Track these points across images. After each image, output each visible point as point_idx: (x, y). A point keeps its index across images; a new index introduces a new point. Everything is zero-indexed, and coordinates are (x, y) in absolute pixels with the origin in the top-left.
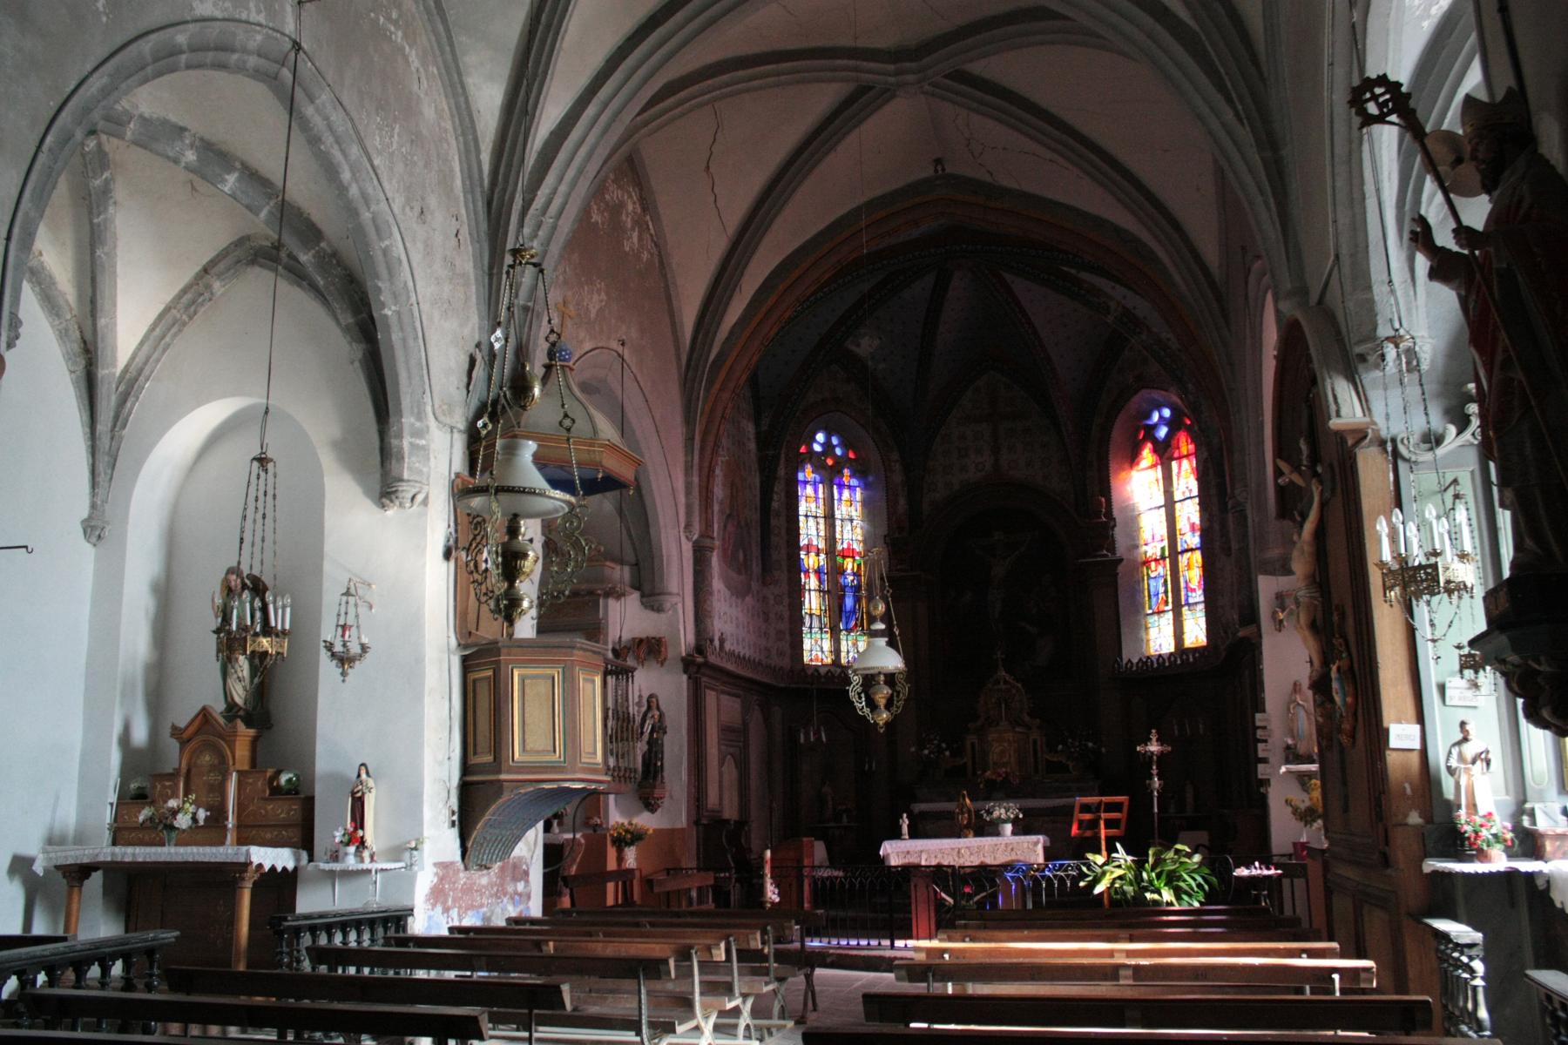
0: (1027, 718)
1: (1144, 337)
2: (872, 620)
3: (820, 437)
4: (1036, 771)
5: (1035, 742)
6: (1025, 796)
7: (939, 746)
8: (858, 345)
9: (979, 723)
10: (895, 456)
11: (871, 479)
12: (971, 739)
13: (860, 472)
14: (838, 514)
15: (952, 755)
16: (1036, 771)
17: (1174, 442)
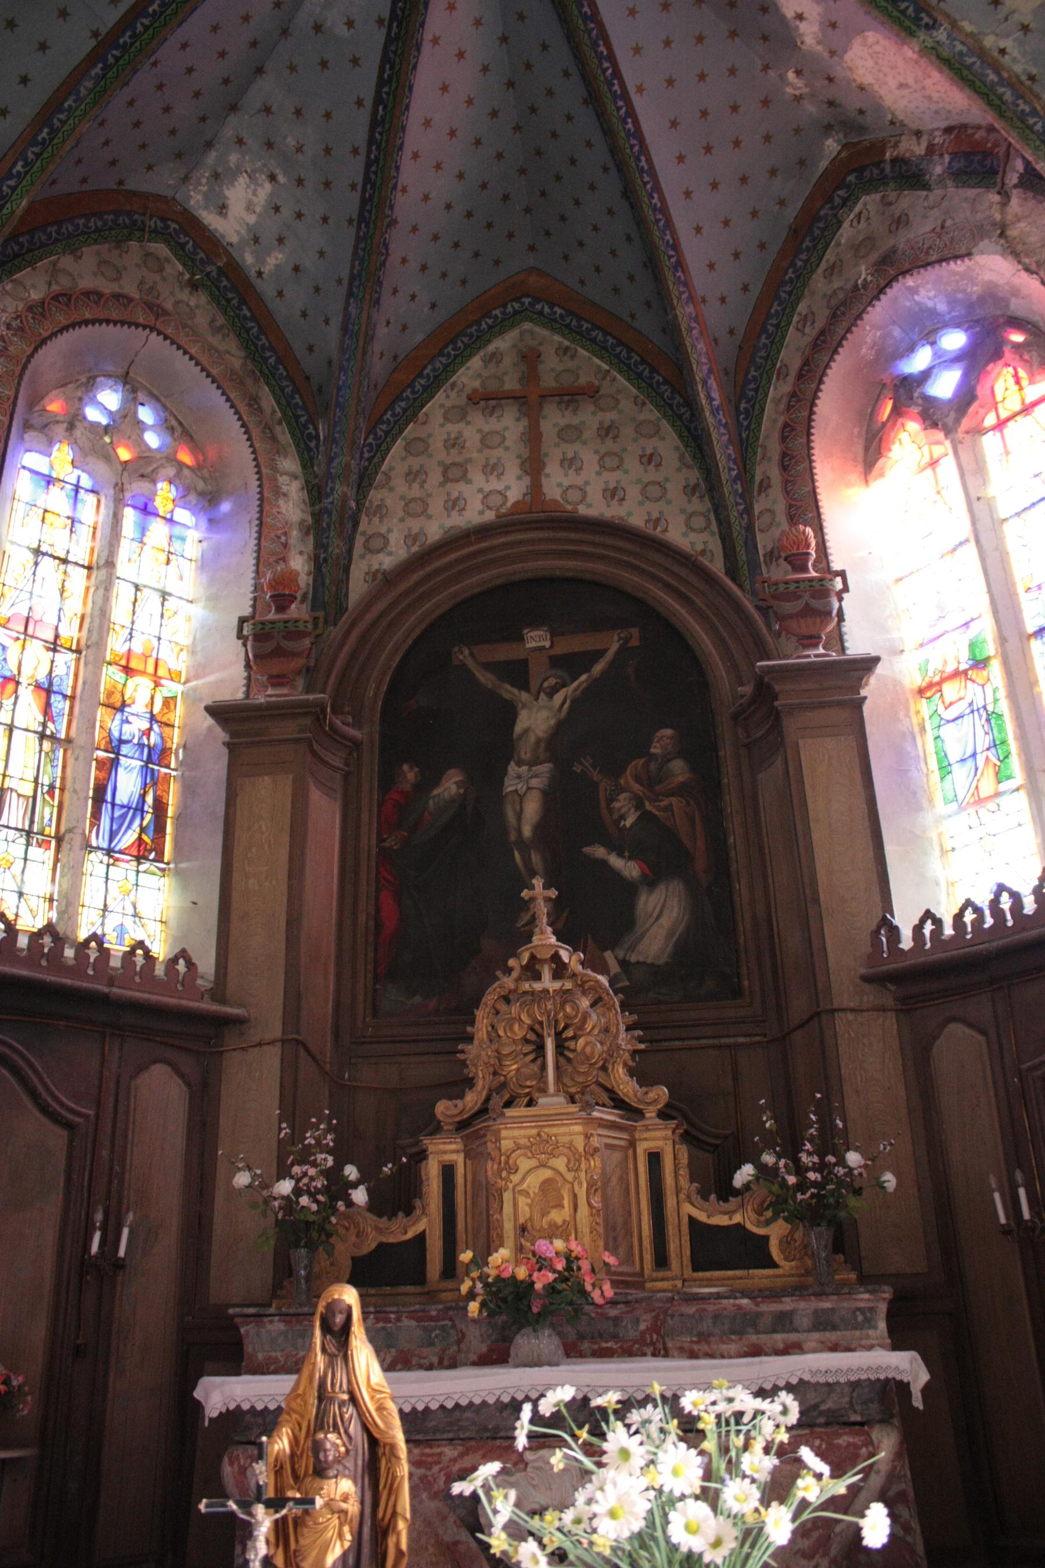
0: (627, 1086)
1: (941, 35)
2: (345, 1216)
3: (110, 398)
4: (661, 1260)
5: (654, 1159)
6: (223, 1513)
7: (333, 1175)
8: (222, 209)
9: (472, 1100)
10: (290, 464)
11: (226, 507)
12: (445, 1150)
13: (206, 493)
14: (123, 568)
15: (375, 1206)
16: (661, 1260)
17: (981, 391)
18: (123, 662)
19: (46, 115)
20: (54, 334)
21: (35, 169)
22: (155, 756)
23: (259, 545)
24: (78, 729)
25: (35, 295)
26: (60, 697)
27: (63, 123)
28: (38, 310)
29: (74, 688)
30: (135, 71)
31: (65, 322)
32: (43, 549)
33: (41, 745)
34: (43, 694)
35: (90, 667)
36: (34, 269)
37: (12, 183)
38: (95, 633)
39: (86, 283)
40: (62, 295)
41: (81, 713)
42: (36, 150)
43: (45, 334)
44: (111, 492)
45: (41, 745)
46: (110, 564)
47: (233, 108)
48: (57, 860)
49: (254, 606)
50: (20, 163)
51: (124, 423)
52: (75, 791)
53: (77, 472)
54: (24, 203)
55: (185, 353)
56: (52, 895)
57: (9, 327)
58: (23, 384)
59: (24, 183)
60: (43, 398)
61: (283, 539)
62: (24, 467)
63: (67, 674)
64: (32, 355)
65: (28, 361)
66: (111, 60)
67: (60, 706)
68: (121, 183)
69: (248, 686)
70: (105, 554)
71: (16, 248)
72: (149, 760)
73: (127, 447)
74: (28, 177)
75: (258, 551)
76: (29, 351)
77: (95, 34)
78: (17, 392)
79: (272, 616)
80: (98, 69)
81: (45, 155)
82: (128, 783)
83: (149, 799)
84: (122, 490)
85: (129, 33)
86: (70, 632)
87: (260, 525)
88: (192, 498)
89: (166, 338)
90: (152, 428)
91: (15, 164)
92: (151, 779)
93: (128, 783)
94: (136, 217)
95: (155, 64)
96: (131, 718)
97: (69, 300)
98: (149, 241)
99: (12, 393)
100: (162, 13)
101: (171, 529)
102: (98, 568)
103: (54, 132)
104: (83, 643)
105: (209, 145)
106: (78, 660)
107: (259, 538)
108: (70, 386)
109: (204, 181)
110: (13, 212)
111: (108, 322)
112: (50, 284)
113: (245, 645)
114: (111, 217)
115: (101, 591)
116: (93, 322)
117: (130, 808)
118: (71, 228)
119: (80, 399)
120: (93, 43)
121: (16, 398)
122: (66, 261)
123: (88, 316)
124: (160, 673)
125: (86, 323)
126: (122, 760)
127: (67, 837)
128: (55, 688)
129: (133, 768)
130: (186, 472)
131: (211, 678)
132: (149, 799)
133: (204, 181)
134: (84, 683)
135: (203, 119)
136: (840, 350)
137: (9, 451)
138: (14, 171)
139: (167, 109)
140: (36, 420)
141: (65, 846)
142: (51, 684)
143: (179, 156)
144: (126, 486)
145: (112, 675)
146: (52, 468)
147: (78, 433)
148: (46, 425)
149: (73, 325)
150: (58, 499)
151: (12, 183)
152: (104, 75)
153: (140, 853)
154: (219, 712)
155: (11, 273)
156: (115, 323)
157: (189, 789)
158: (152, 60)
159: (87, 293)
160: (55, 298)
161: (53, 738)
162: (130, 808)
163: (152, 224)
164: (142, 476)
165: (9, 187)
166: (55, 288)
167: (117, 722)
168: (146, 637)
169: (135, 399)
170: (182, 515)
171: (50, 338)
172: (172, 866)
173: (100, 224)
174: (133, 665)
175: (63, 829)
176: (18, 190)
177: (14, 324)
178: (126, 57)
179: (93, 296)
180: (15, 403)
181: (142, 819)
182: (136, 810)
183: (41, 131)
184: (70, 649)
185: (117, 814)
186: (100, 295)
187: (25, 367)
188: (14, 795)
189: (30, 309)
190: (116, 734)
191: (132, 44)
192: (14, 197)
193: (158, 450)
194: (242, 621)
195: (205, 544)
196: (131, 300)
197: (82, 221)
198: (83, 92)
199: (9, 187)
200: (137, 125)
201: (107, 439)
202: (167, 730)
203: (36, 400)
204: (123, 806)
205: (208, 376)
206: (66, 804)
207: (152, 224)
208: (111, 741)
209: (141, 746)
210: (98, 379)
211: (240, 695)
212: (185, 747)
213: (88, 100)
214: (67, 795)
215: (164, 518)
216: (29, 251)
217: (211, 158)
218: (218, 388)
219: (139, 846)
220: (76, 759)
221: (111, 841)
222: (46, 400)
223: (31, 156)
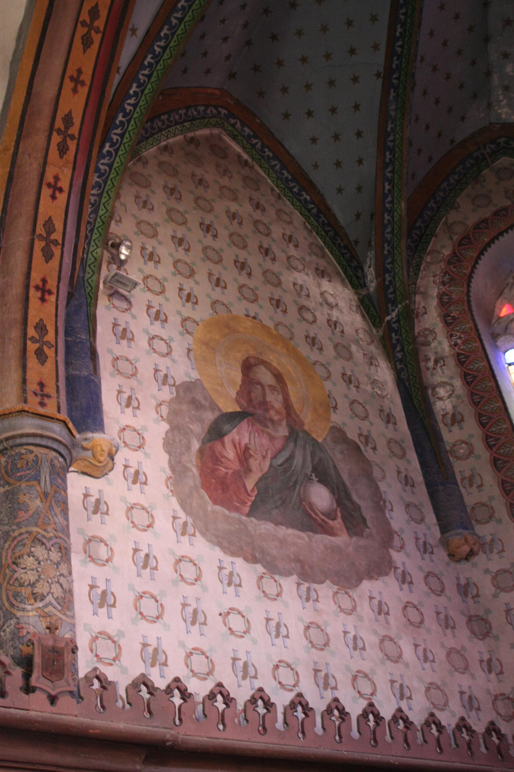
19: (382, 146)
20: (474, 267)
21: (396, 181)
25: (447, 252)
27: (394, 141)
28: (455, 260)
30: (413, 76)
31: (475, 255)
36: (436, 236)
37: (389, 199)
39: (472, 220)
40: (462, 239)
42: (390, 169)
43: (467, 272)
47: (487, 40)
50: (386, 184)
54: (403, 205)
57: (443, 284)
58: (475, 313)
59: (396, 194)
60: (493, 311)
62: (510, 365)
64: (468, 291)
65: (469, 296)
66: (395, 82)
68: (452, 142)
71: (418, 232)
74: (396, 189)
76: (465, 290)
77: (378, 75)
78: (474, 320)
80: (392, 94)
81: (397, 168)
85: (395, 58)
91: (384, 187)
94: (476, 154)
95: (422, 59)
97: (469, 239)
98: (493, 162)
99: (471, 324)
100: (405, 30)
103: (392, 151)
105: (489, 74)
108: (506, 290)
109: (501, 97)
110: (400, 216)
111: (501, 234)
112: (451, 238)
114: (461, 167)
116: (492, 241)
118: (441, 194)
120: (380, 80)
121: (476, 325)
122: (453, 216)
123: (486, 240)
125: (488, 245)
133: (501, 97)
135: (473, 63)
136: (479, 261)
137: (492, 363)
138: (386, 191)
139: (448, 77)
140: (498, 329)
143: (475, 96)
148: (506, 328)
149: (482, 253)
151: (389, 199)
152: (398, 94)
155: (425, 249)
156: (506, 231)
158: (419, 58)
159: (477, 226)
160: (460, 244)
163: (488, 150)
165: (389, 203)
166: (455, 238)
171: (472, 272)
173: (456, 177)
176: (395, 201)
177: (446, 280)
178: (403, 73)
179: (482, 225)
180: (477, 330)
183: (385, 155)
186: (485, 221)
187: (469, 301)
189: (449, 263)
191: (401, 63)
192: (396, 206)
196: (506, 209)
197: (445, 185)
198: (393, 113)
199: (389, 203)
200: (437, 102)
203: (490, 316)
207: (488, 150)
213: (399, 116)
216: (426, 227)
217: (495, 80)
222: (497, 310)
223: (389, 175)
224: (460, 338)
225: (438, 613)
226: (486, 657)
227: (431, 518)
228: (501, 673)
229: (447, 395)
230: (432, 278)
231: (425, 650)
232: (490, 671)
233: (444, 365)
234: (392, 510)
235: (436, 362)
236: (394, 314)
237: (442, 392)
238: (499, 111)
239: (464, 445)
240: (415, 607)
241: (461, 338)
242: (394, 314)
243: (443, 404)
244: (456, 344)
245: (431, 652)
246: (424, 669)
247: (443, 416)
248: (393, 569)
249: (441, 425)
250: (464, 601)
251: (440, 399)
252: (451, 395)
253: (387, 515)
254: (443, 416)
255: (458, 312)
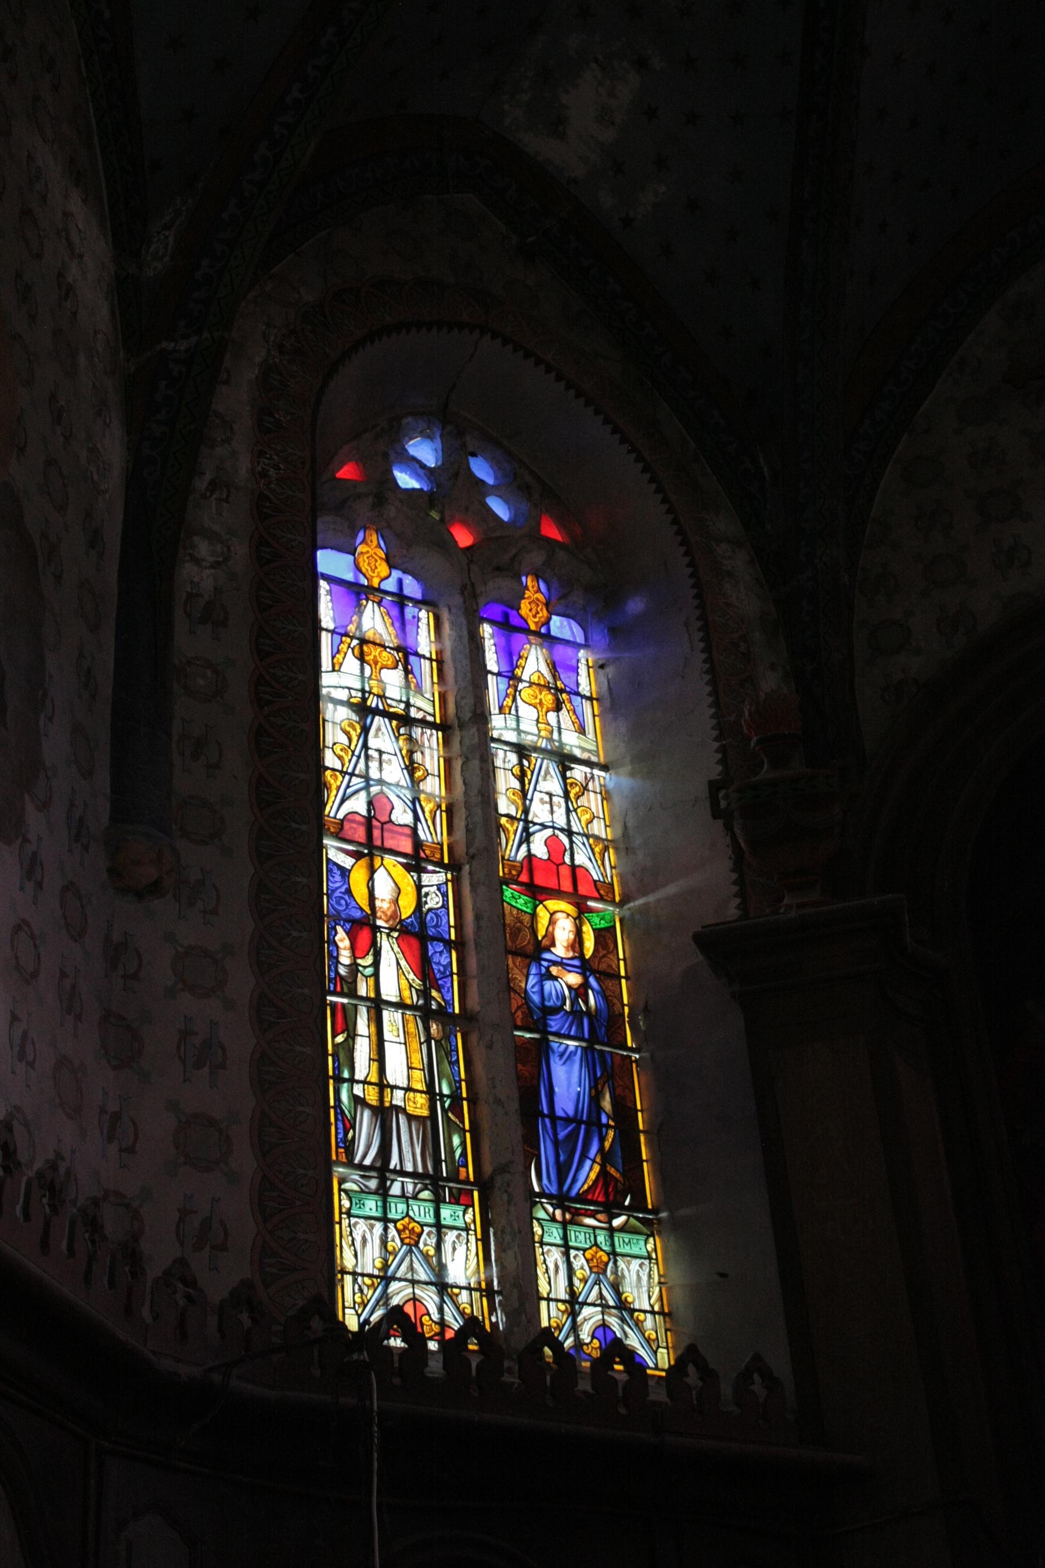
11: (636, 606)
18: (524, 878)
22: (600, 1030)
23: (709, 660)
24: (481, 995)
26: (440, 947)
29: (459, 927)
32: (372, 702)
33: (427, 1029)
34: (415, 943)
35: (482, 889)
38: (479, 834)
41: (482, 968)
44: (458, 600)
45: (427, 1029)
46: (481, 717)
48: (486, 1224)
49: (723, 762)
51: (450, 485)
52: (498, 1102)
53: (396, 574)
55: (539, 362)
56: (489, 1283)
61: (743, 646)
63: (445, 906)
67: (444, 961)
69: (742, 894)
70: (469, 701)
72: (593, 1040)
73: (465, 523)
75: (711, 671)
79: (766, 772)
82: (568, 1082)
83: (607, 1104)
84: (475, 596)
86: (433, 833)
87: (705, 628)
88: (578, 598)
89: (506, 342)
90: (495, 490)
92: (605, 1073)
93: (568, 1082)
96: (554, 970)
101: (550, 650)
102: (461, 726)
104: (461, 850)
106: (456, 882)
107: (707, 649)
113: (729, 828)
115: (475, 764)
117: (580, 1122)
119: (386, 455)
124: (582, 890)
126: (555, 1042)
127: (499, 1181)
128: (431, 932)
129: (573, 1054)
130: (561, 555)
131: (671, 890)
132: (607, 1104)
134: (478, 917)
141: (499, 1198)
142: (423, 923)
144: (480, 588)
145: (515, 899)
146: (358, 568)
147: (391, 511)
150: (373, 620)
153: (609, 1197)
154: (712, 942)
157: (667, 1081)
161: (442, 1014)
162: (580, 1122)
164: (498, 569)
167: (532, 980)
168: (549, 832)
169: (464, 446)
170: (559, 626)
172: (663, 1215)
174: (539, 880)
175: (488, 1169)
181: (602, 1140)
182: (589, 1124)
184: (440, 864)
185: (562, 1134)
188: (402, 1119)
190: (536, 998)
193: (512, 522)
194: (714, 787)
195: (610, 670)
201: (435, 515)
202: (610, 983)
204: (567, 1120)
205: (578, 395)
206: (485, 1125)
208: (530, 1011)
209: (576, 1014)
210: (405, 421)
211: (732, 912)
212: (646, 1010)
214: (484, 1110)
215: (537, 634)
218: (597, 412)
219: (606, 1185)
220: (490, 1046)
221: (561, 1182)
224: (277, 467)
225: (63, 975)
226: (112, 1107)
227: (103, 779)
228: (131, 1150)
229: (212, 559)
230: (264, 327)
231: (25, 1034)
232: (110, 1139)
233: (227, 501)
234: (50, 719)
235: (213, 485)
236: (183, 345)
237: (203, 548)
238: (506, 107)
239: (209, 672)
240: (32, 937)
241: (279, 469)
242: (183, 345)
243: (199, 572)
244: (264, 474)
245: (33, 1044)
246: (13, 1072)
247: (190, 595)
248: (19, 841)
249: (179, 612)
250: (106, 976)
251: (197, 561)
252: (218, 563)
253: (42, 724)
254: (190, 595)
255: (289, 417)
